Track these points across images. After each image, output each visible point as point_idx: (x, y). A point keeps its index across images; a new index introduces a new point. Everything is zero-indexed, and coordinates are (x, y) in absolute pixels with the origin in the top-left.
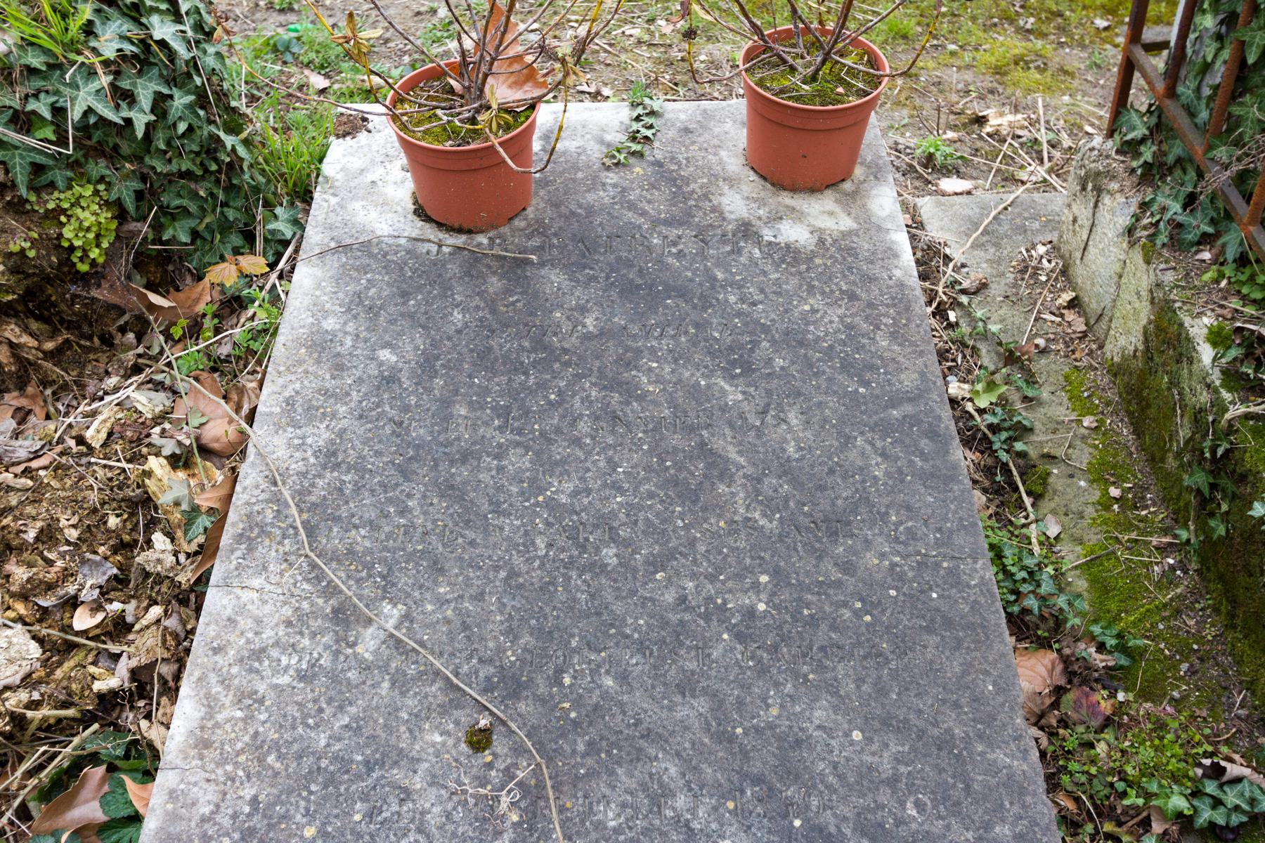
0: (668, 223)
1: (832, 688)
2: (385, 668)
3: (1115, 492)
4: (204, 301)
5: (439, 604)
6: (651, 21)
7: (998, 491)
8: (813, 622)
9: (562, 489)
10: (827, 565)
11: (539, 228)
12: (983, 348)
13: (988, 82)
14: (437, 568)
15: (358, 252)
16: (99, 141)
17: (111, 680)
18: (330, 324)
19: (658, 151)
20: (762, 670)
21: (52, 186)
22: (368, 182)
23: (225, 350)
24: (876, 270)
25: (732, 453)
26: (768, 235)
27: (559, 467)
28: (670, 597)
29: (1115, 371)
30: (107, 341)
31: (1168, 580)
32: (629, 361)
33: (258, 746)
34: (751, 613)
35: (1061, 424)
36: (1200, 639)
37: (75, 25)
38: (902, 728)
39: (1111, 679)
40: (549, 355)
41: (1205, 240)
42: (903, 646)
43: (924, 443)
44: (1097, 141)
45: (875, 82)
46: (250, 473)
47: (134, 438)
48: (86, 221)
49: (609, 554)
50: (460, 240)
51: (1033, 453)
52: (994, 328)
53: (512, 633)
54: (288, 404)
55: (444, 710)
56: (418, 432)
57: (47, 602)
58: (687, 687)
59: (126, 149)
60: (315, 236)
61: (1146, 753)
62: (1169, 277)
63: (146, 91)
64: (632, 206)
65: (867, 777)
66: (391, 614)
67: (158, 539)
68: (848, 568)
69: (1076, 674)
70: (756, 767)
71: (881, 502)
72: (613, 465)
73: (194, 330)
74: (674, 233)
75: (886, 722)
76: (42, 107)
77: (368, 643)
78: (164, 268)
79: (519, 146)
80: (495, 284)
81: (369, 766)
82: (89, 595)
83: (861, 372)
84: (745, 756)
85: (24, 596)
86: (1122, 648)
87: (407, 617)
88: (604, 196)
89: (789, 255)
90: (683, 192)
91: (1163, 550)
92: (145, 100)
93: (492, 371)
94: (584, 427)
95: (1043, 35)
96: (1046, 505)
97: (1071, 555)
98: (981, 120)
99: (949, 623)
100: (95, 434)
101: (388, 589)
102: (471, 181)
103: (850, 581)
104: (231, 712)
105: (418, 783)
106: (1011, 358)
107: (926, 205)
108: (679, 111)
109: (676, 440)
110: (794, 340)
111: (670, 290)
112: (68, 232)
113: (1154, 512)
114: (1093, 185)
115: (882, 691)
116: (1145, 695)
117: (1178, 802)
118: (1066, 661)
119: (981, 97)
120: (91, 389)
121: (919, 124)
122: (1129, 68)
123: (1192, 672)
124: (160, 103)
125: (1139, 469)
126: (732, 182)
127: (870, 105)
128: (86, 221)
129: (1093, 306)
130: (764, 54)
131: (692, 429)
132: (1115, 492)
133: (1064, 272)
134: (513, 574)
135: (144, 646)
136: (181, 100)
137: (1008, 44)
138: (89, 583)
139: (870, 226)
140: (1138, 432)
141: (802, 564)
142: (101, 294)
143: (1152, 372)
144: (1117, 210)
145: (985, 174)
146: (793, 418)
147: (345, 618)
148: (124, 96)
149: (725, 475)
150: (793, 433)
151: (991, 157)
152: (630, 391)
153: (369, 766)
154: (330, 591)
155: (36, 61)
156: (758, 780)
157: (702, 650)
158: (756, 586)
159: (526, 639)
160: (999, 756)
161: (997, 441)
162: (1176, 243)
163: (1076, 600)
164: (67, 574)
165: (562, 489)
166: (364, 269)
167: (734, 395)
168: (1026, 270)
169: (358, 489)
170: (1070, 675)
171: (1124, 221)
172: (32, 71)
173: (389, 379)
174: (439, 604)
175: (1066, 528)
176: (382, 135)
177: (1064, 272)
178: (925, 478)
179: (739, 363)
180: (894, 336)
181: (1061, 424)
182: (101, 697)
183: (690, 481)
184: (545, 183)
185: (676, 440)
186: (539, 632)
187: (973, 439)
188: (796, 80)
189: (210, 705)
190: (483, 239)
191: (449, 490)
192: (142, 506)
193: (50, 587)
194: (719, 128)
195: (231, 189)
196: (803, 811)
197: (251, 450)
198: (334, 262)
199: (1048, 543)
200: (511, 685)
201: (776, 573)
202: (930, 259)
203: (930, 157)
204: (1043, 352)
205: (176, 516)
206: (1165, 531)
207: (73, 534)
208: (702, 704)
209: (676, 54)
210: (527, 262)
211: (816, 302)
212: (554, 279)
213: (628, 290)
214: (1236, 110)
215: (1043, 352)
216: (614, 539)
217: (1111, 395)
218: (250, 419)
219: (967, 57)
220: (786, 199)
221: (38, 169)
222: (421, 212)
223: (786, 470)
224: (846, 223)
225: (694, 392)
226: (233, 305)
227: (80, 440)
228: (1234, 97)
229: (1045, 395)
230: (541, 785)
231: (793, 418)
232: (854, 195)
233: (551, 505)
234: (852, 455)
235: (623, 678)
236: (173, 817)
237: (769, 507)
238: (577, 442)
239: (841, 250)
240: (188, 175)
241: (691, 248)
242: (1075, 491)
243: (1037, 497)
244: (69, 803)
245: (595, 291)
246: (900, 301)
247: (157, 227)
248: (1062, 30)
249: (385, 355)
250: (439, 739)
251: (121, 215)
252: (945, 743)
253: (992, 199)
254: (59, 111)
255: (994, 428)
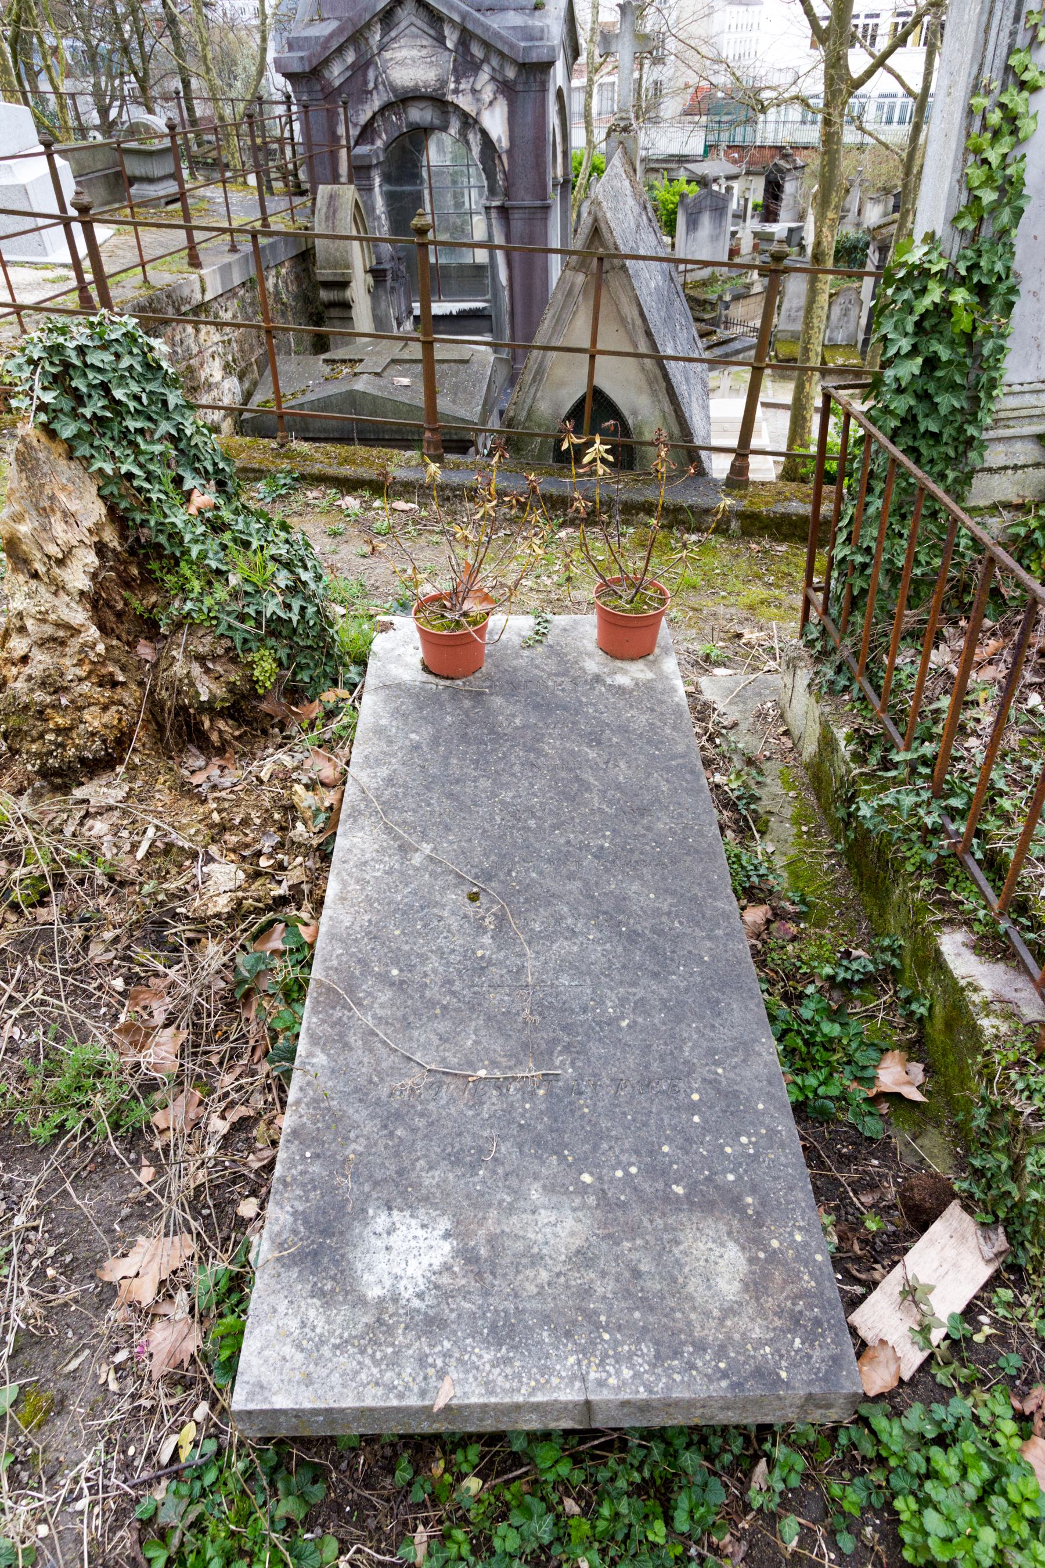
0: (557, 675)
1: (641, 878)
2: (426, 869)
3: (804, 829)
4: (316, 710)
5: (450, 844)
6: (538, 577)
7: (742, 831)
8: (632, 851)
9: (507, 796)
10: (639, 827)
11: (489, 677)
12: (735, 758)
13: (745, 614)
14: (448, 829)
15: (393, 689)
16: (276, 628)
17: (282, 890)
18: (384, 722)
19: (550, 640)
20: (607, 870)
21: (250, 650)
22: (398, 651)
23: (327, 736)
24: (665, 698)
25: (592, 780)
26: (609, 681)
27: (506, 786)
28: (562, 841)
29: (807, 767)
30: (265, 732)
31: (832, 870)
32: (539, 739)
33: (369, 900)
34: (602, 847)
35: (777, 795)
36: (847, 899)
37: (268, 574)
38: (674, 893)
39: (797, 918)
40: (496, 736)
41: (846, 689)
42: (674, 861)
43: (688, 776)
44: (794, 641)
45: (663, 602)
46: (350, 789)
47: (285, 779)
48: (265, 667)
49: (532, 823)
50: (448, 683)
51: (761, 811)
52: (740, 746)
53: (486, 855)
54: (1009, 180)
55: (456, 886)
56: (433, 771)
57: (246, 853)
58: (571, 877)
59: (285, 633)
60: (370, 679)
61: (813, 950)
62: (828, 709)
63: (296, 604)
64: (537, 667)
65: (657, 912)
66: (427, 848)
67: (299, 824)
68: (649, 829)
69: (778, 915)
70: (604, 908)
71: (665, 802)
72: (532, 785)
73: (312, 726)
74: (560, 680)
75: (666, 891)
76: (251, 611)
77: (417, 859)
78: (295, 694)
79: (481, 632)
80: (467, 703)
81: (422, 908)
82: (266, 850)
83: (657, 744)
84: (599, 903)
85: (234, 851)
86: (803, 901)
87: (435, 849)
88: (521, 662)
89: (621, 690)
90: (565, 663)
91: (829, 856)
92: (296, 608)
93: (469, 743)
94: (517, 768)
95: (780, 587)
96: (767, 837)
97: (779, 862)
98: (739, 636)
99: (697, 851)
100: (265, 775)
101: (424, 836)
102: (453, 652)
103: (650, 835)
104: (353, 886)
105: (446, 914)
106: (750, 762)
107: (704, 682)
108: (561, 620)
109: (563, 774)
110: (623, 729)
111: (557, 707)
112: (256, 673)
113: (826, 838)
114: (792, 665)
115: (664, 878)
116: (816, 925)
117: (828, 970)
118: (773, 909)
119: (740, 623)
120: (259, 754)
121: (702, 638)
122: (807, 602)
123: (841, 914)
124: (303, 609)
125: (818, 818)
126: (590, 655)
127: (662, 613)
128: (265, 667)
129: (796, 733)
130: (606, 589)
131: (571, 770)
132: (804, 829)
133: (782, 716)
134: (485, 831)
135: (295, 875)
136: (311, 610)
137: (757, 592)
138: (267, 844)
139: (663, 677)
140: (818, 799)
141: (627, 827)
142: (264, 706)
143: (822, 762)
144: (804, 676)
145: (741, 666)
146: (622, 765)
147: (405, 849)
148: (288, 607)
149: (588, 789)
150: (622, 772)
151: (735, 651)
152: (539, 753)
153: (422, 908)
154: (397, 837)
155: (249, 589)
156: (606, 913)
157: (579, 862)
158: (604, 836)
159: (493, 858)
160: (719, 904)
161: (741, 804)
162: (831, 692)
163: (780, 882)
164: (256, 841)
165: (507, 796)
166: (398, 697)
167: (592, 755)
168: (762, 716)
169: (405, 795)
170: (775, 915)
171: (806, 682)
172: (246, 593)
173: (416, 747)
174: (450, 844)
175: (775, 850)
176: (406, 626)
177: (782, 716)
178: (688, 791)
179: (595, 740)
180: (674, 728)
181: (777, 795)
182: (274, 898)
183: (572, 792)
184: (491, 655)
185: (563, 774)
186: (500, 855)
187: (727, 803)
188: (622, 602)
189: (344, 884)
190: (460, 682)
191: (451, 796)
192: (290, 808)
193: (247, 846)
194: (584, 629)
195: (329, 656)
196: (627, 925)
197: (350, 779)
198: (383, 693)
199: (769, 857)
200: (488, 876)
201: (614, 831)
202: (702, 711)
203: (708, 656)
204: (769, 759)
205: (309, 814)
206: (831, 846)
207: (258, 821)
208: (579, 884)
209: (553, 596)
210: (483, 693)
211: (634, 712)
212: (498, 701)
213: (537, 707)
214: (852, 619)
215: (769, 759)
216: (533, 815)
217: (806, 780)
218: (348, 763)
219: (732, 599)
220: (618, 664)
221: (245, 641)
222: (426, 669)
223: (618, 787)
224: (650, 675)
225: (572, 753)
226: (330, 715)
227: (258, 778)
228: (851, 613)
229: (768, 781)
230: (504, 915)
231: (622, 765)
232: (654, 662)
233: (502, 802)
234: (652, 781)
235: (541, 873)
236: (333, 927)
237: (610, 803)
238: (514, 775)
239: (648, 687)
240: (310, 647)
241: (569, 687)
242: (784, 829)
243: (763, 833)
244: (268, 939)
245: (518, 706)
246: (677, 712)
247: (294, 674)
248: (791, 583)
249: (413, 736)
250: (455, 897)
251: (280, 664)
252: (694, 899)
253: (743, 678)
254: (258, 613)
255: (739, 798)
